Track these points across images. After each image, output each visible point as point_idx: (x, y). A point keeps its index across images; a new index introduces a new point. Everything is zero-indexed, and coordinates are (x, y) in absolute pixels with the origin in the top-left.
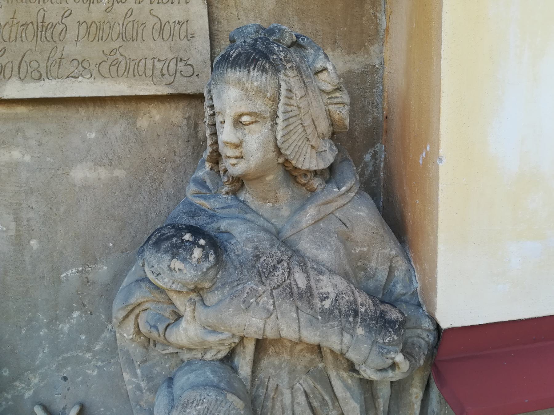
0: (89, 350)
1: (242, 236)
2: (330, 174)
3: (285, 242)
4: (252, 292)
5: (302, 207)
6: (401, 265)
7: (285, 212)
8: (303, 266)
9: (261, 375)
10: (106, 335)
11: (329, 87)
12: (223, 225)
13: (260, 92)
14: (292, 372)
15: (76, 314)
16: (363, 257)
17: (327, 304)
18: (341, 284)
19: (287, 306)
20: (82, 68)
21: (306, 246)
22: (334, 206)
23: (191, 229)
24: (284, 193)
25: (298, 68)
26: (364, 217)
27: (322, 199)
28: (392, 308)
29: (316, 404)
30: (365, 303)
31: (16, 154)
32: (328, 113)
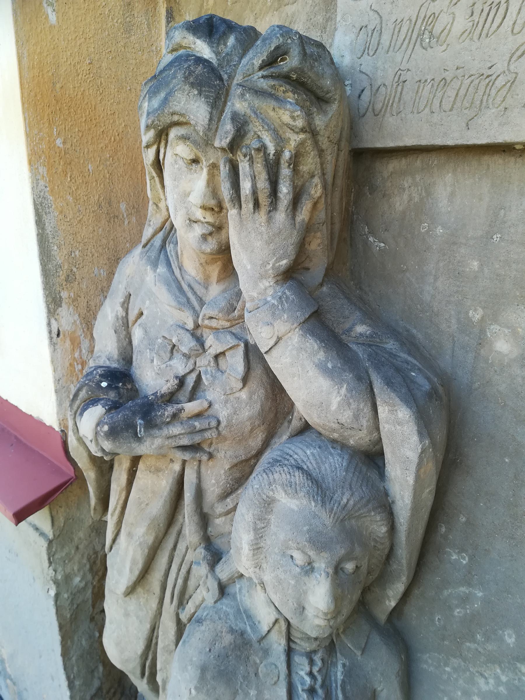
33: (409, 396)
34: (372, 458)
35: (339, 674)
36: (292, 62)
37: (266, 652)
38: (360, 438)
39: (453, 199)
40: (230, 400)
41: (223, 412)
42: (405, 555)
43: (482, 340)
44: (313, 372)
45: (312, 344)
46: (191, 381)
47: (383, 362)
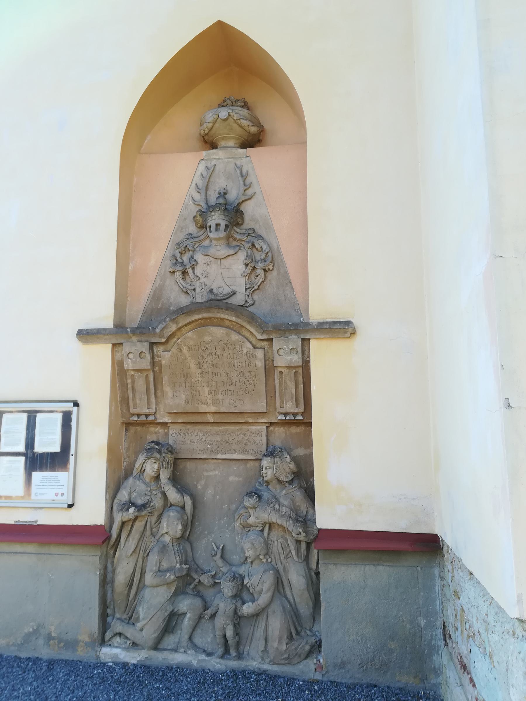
0: (227, 529)
1: (266, 495)
2: (291, 482)
3: (276, 499)
4: (266, 508)
5: (282, 491)
6: (311, 511)
7: (278, 491)
8: (279, 504)
9: (270, 537)
10: (232, 525)
11: (289, 461)
12: (262, 493)
13: (270, 462)
14: (278, 536)
15: (225, 518)
16: (299, 506)
17: (283, 513)
18: (288, 510)
19: (273, 512)
20: (236, 452)
21: (282, 500)
22: (291, 491)
23: (255, 493)
24: (278, 486)
25: (280, 457)
26: (299, 496)
27: (287, 489)
28: (306, 521)
29: (283, 547)
30: (293, 515)
31: (217, 472)
32: (289, 467)
33: (188, 495)
34: (183, 508)
35: (181, 547)
36: (170, 449)
37: (169, 547)
38: (181, 504)
39: (190, 465)
40: (158, 502)
41: (157, 505)
42: (189, 523)
43: (197, 487)
44: (175, 493)
45: (174, 488)
46: (150, 500)
47: (184, 491)
